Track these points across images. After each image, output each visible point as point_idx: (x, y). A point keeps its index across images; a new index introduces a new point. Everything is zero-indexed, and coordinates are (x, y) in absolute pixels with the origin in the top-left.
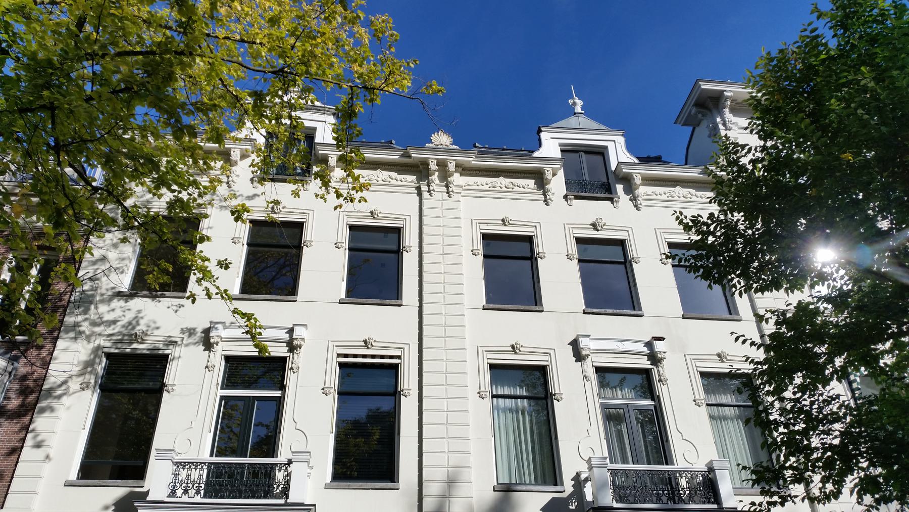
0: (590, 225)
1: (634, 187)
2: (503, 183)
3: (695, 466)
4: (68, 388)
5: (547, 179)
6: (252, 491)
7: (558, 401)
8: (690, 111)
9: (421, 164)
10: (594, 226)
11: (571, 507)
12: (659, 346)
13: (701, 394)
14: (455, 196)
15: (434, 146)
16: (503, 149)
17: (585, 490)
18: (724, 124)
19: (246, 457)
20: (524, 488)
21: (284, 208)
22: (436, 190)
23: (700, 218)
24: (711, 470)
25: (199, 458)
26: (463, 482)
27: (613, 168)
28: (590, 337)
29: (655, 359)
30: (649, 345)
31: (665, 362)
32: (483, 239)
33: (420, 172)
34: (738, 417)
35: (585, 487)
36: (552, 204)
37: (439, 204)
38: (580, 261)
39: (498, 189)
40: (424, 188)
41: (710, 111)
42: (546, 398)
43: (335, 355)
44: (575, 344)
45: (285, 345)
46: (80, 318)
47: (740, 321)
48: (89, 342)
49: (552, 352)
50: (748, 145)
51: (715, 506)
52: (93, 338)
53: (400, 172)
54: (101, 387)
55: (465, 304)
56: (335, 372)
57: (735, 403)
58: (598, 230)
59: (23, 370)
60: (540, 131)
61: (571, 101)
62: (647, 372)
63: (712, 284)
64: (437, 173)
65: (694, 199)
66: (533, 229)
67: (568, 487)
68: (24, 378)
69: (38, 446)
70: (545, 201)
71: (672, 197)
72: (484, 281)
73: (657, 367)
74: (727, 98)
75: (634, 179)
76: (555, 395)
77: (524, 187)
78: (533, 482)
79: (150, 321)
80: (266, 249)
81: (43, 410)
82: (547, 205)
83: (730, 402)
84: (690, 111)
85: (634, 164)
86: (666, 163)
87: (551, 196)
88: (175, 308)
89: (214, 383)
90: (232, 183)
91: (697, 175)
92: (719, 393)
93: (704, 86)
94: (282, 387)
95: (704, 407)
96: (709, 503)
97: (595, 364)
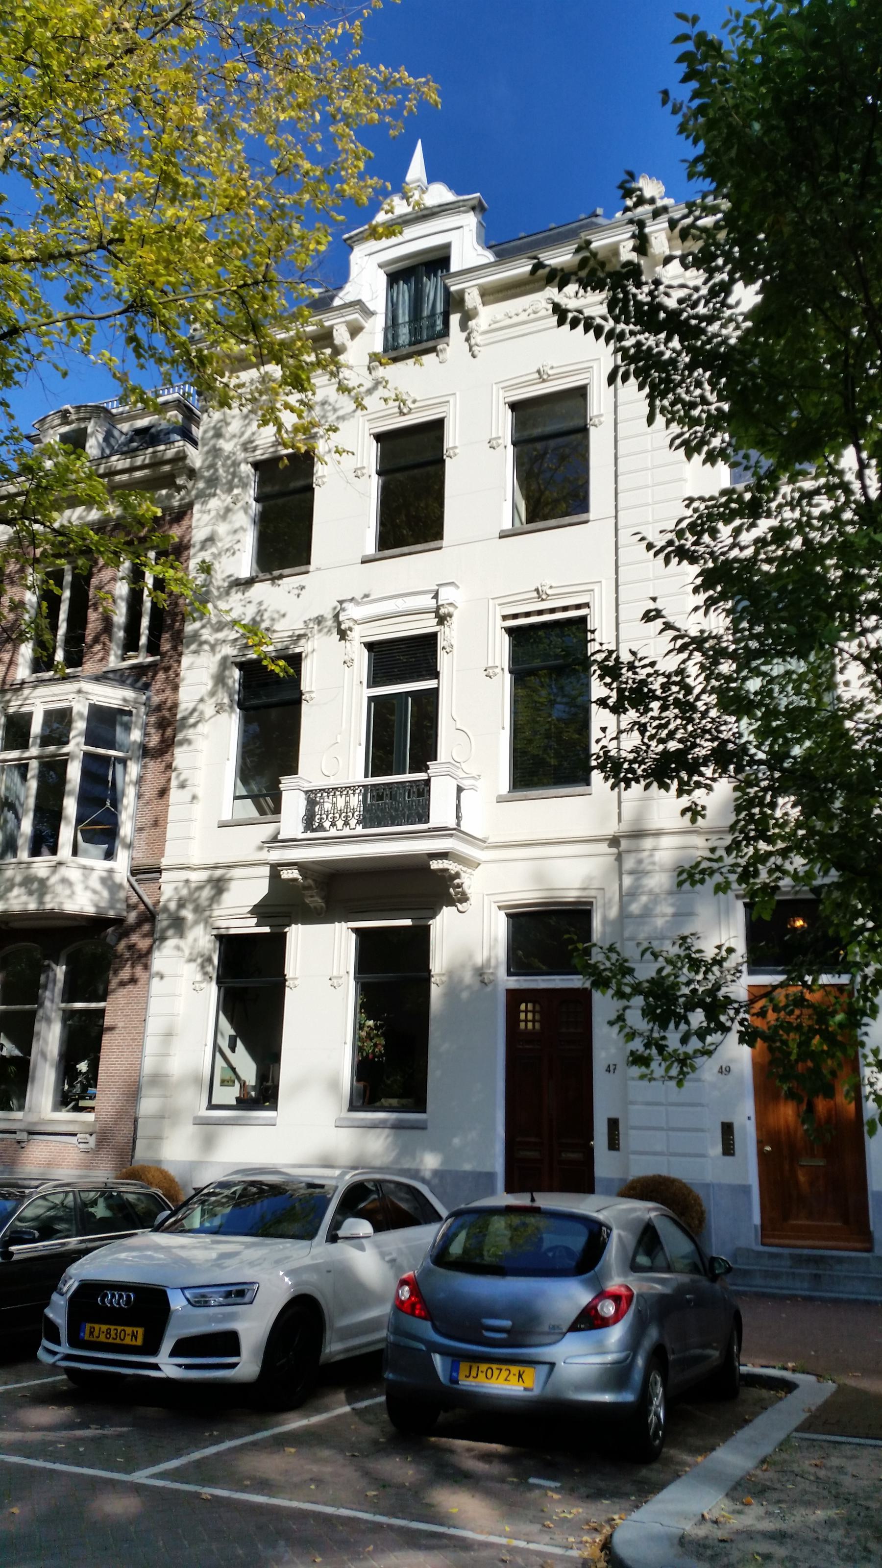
4: (202, 713)
6: (392, 817)
10: (540, 374)
19: (404, 773)
21: (414, 402)
25: (350, 780)
43: (499, 618)
45: (433, 615)
46: (197, 625)
48: (214, 654)
52: (218, 648)
54: (240, 705)
56: (504, 643)
59: (156, 700)
68: (159, 708)
69: (182, 786)
71: (535, 313)
79: (273, 612)
80: (560, 440)
81: (181, 743)
88: (297, 592)
89: (356, 682)
94: (436, 675)
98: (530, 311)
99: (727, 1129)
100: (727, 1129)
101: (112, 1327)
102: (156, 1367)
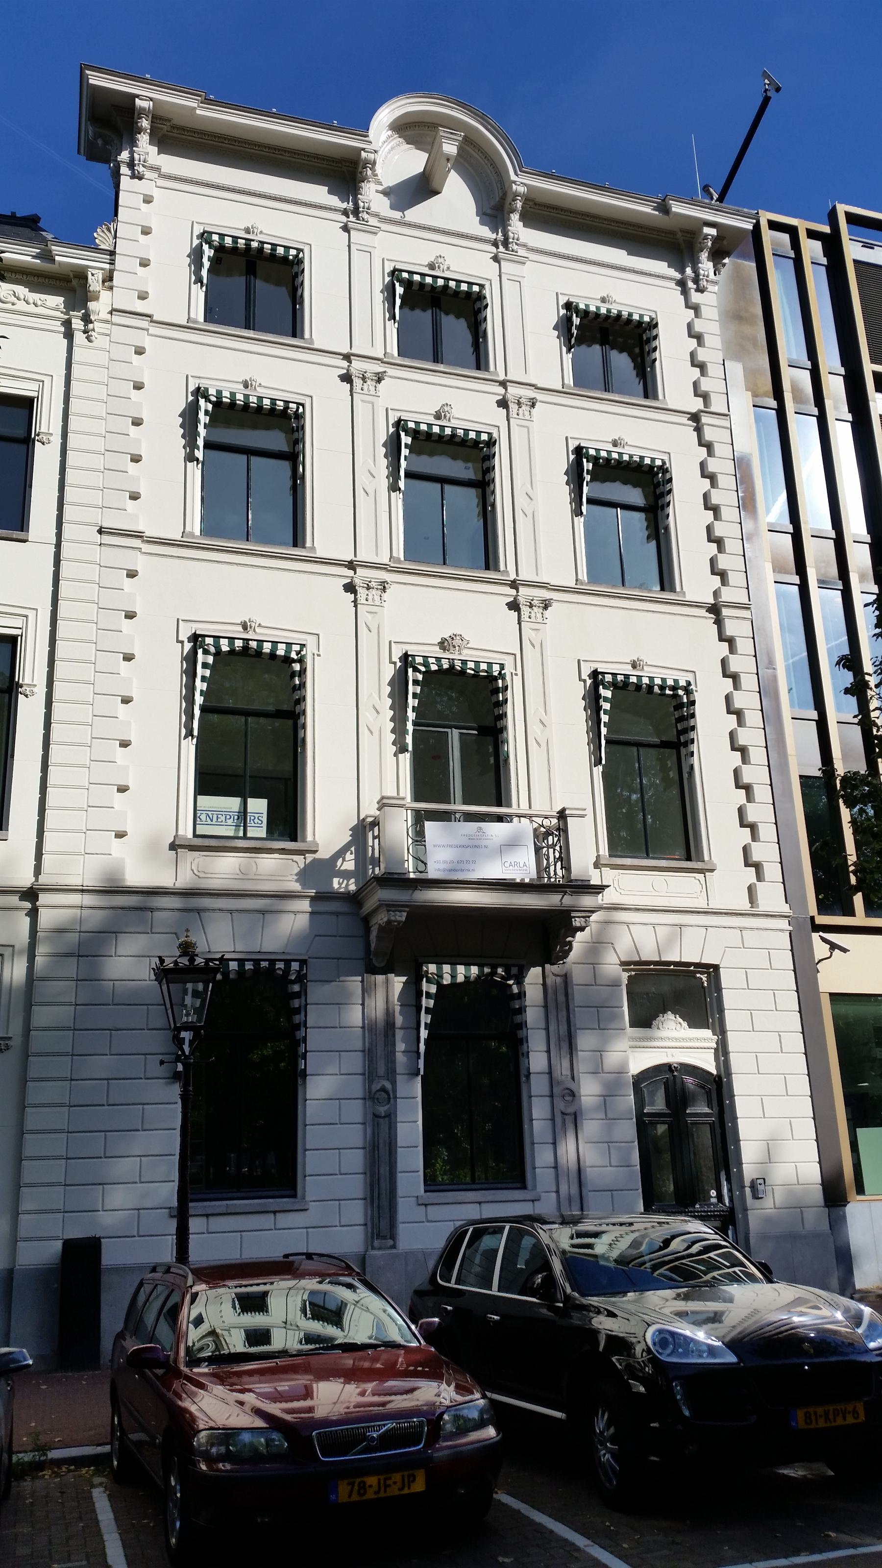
33: (73, 290)
66: (35, 386)
91: (29, 259)
93: (96, 80)
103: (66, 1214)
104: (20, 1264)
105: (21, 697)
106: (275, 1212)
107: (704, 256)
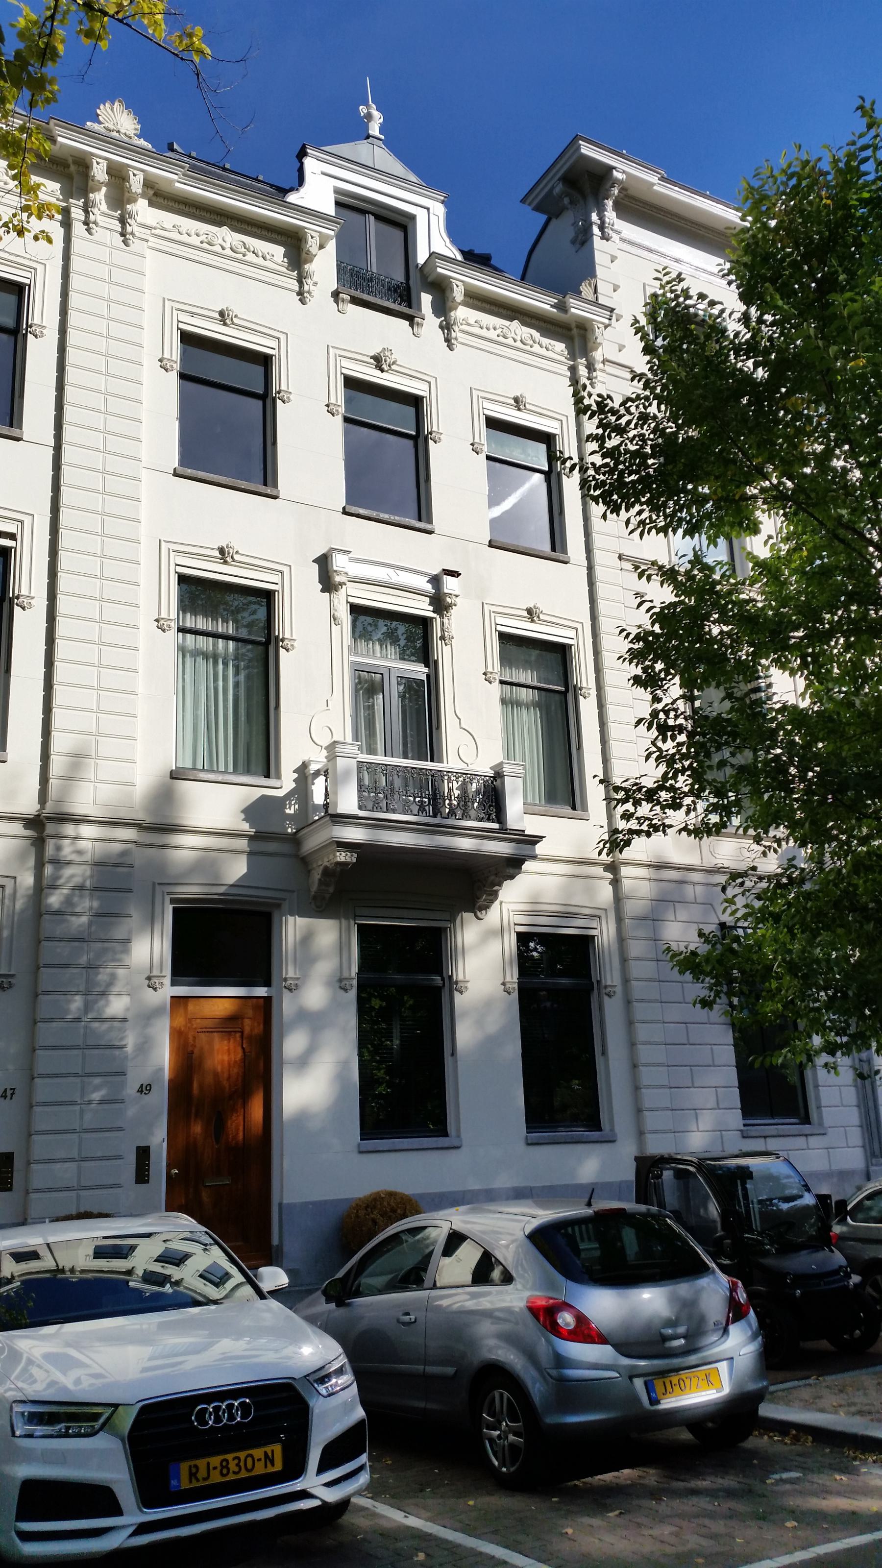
0: (372, 357)
1: (449, 304)
2: (228, 239)
3: (470, 767)
5: (308, 253)
7: (287, 650)
8: (553, 188)
9: (577, 327)
10: (378, 362)
11: (288, 811)
12: (450, 584)
13: (494, 664)
14: (136, 245)
15: (103, 131)
16: (224, 169)
17: (313, 787)
18: (602, 227)
20: (211, 777)
22: (137, 234)
23: (609, 401)
24: (498, 775)
26: (98, 757)
27: (422, 257)
28: (351, 555)
29: (440, 603)
30: (435, 581)
31: (454, 611)
32: (181, 342)
34: (537, 705)
35: (313, 784)
36: (311, 302)
37: (104, 253)
38: (183, 376)
39: (217, 249)
40: (77, 214)
41: (584, 197)
42: (267, 643)
44: (324, 562)
47: (566, 563)
49: (286, 570)
50: (721, 303)
51: (496, 826)
53: (545, 333)
55: (143, 459)
57: (535, 683)
58: (382, 371)
60: (302, 154)
61: (363, 110)
62: (425, 622)
63: (608, 512)
64: (104, 189)
65: (536, 348)
67: (287, 782)
70: (300, 293)
71: (505, 337)
72: (177, 423)
73: (442, 616)
74: (616, 181)
75: (452, 290)
76: (282, 640)
77: (264, 258)
78: (231, 769)
82: (303, 301)
83: (529, 682)
84: (553, 188)
85: (453, 261)
86: (497, 271)
87: (312, 288)
90: (131, 237)
91: (548, 307)
92: (517, 668)
93: (587, 150)
95: (496, 685)
96: (488, 820)
97: (351, 600)
98: (203, 238)
99: (143, 1153)
100: (143, 1153)
101: (229, 1457)
102: (304, 1495)
103: (84, 1164)
104: (33, 1216)
105: (282, 651)
106: (765, 1137)
107: (609, 203)
